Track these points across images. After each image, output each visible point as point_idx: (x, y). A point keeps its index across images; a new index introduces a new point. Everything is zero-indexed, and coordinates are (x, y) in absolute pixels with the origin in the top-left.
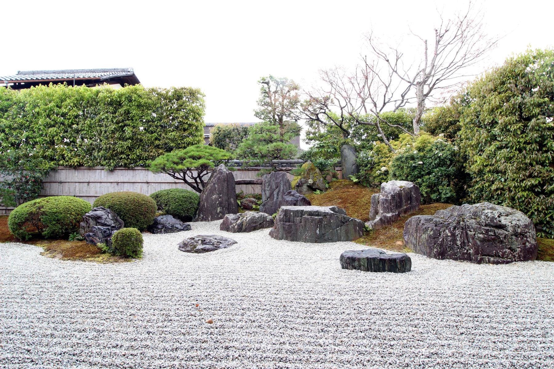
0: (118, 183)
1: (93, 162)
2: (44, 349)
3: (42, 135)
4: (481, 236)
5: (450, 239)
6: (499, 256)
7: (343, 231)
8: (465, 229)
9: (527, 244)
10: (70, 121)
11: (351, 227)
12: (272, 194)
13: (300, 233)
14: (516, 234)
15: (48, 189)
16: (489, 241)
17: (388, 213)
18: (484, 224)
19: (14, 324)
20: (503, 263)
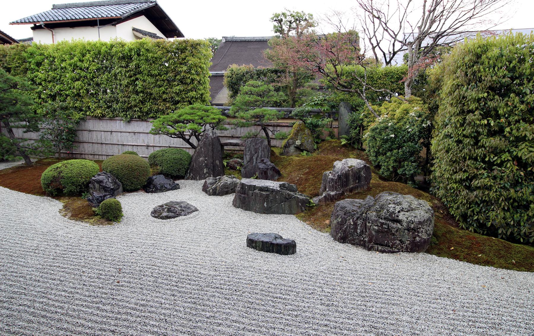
0: (135, 133)
1: (113, 113)
2: (32, 288)
3: (70, 88)
4: (376, 228)
5: (352, 227)
6: (389, 246)
7: (287, 206)
8: (366, 220)
9: (417, 238)
10: (91, 75)
11: (294, 202)
12: (251, 159)
13: (252, 204)
14: (409, 229)
15: (80, 136)
16: (382, 232)
17: (333, 191)
18: (383, 217)
19: (25, 270)
20: (389, 252)
